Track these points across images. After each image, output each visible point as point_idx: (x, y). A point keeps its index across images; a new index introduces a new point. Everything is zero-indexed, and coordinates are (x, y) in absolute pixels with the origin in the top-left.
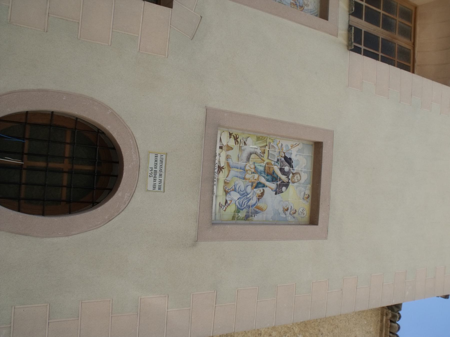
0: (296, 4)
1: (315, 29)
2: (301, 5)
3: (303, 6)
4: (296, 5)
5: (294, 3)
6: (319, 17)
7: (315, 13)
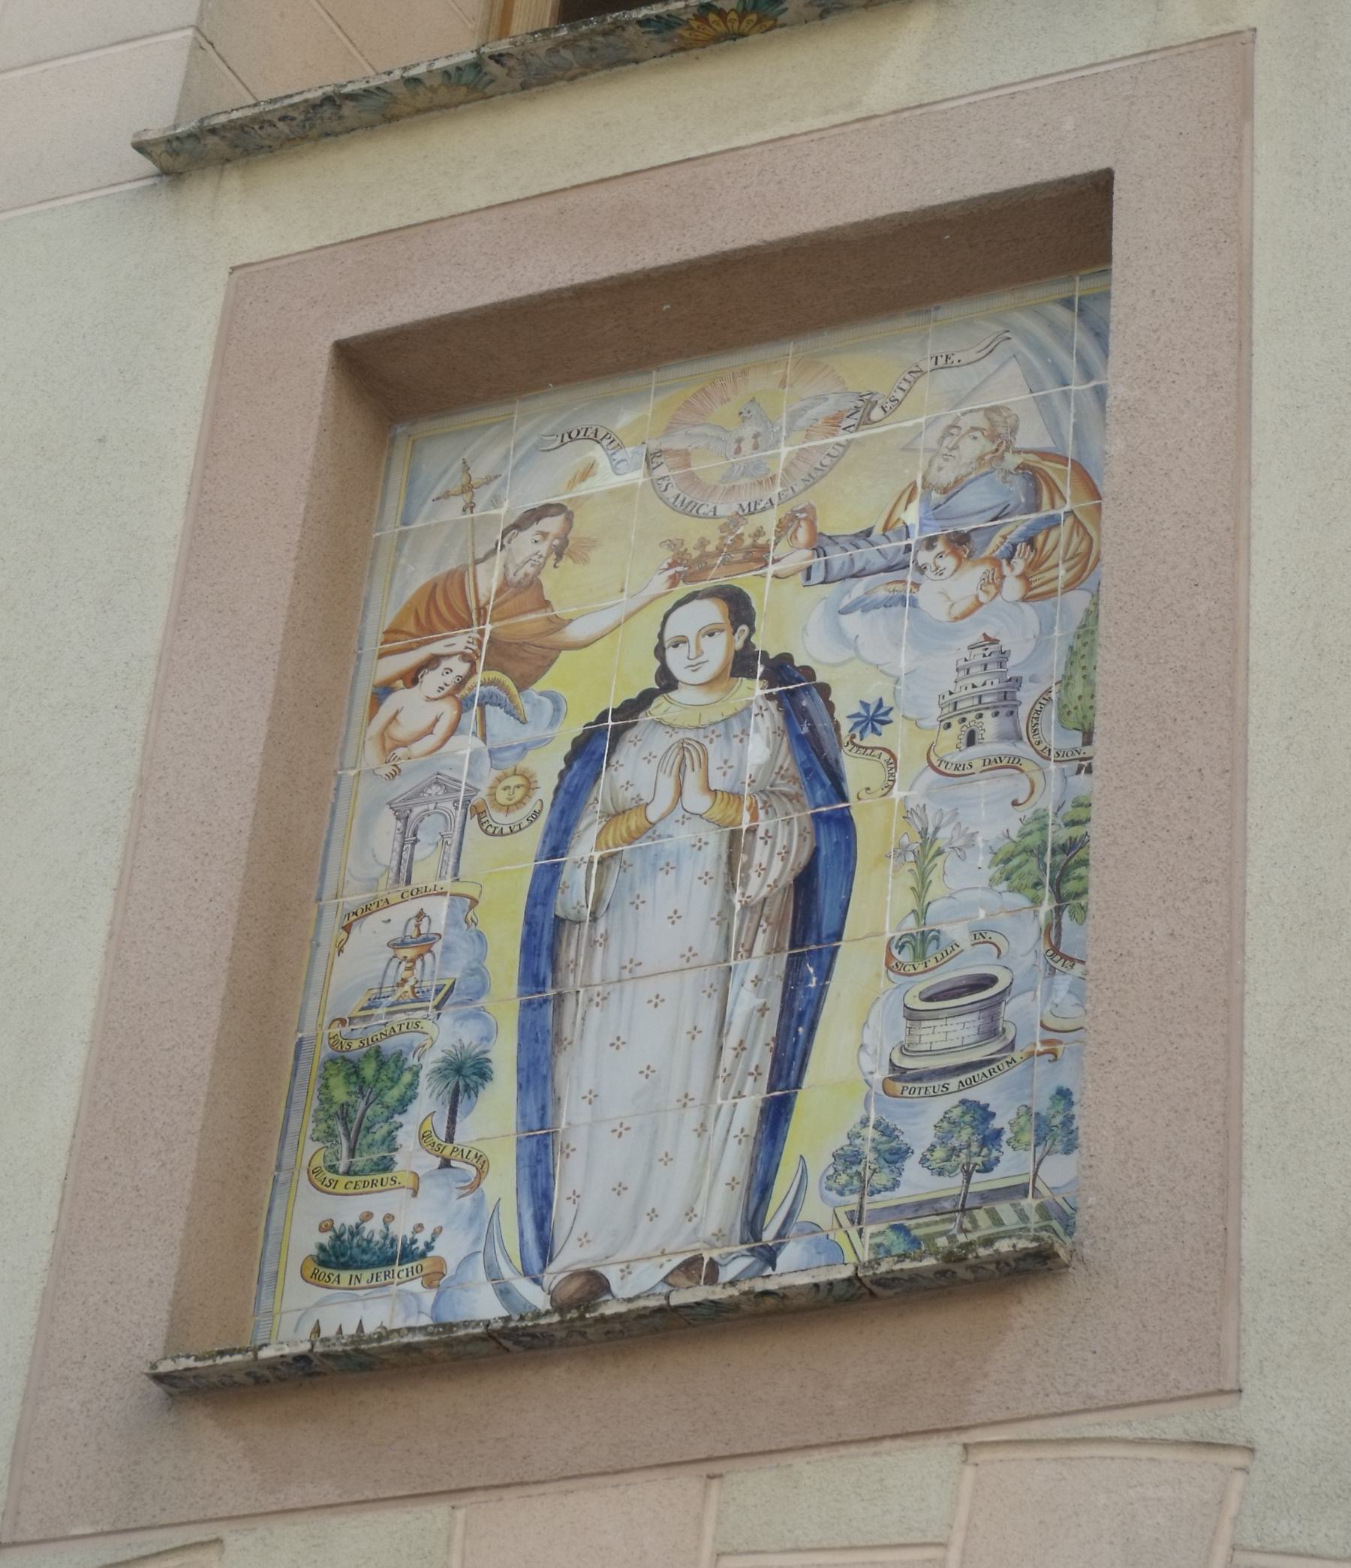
0: (1031, 542)
1: (1243, 278)
2: (1017, 490)
3: (1022, 467)
4: (1040, 538)
5: (1019, 565)
6: (1108, 272)
7: (1052, 325)
